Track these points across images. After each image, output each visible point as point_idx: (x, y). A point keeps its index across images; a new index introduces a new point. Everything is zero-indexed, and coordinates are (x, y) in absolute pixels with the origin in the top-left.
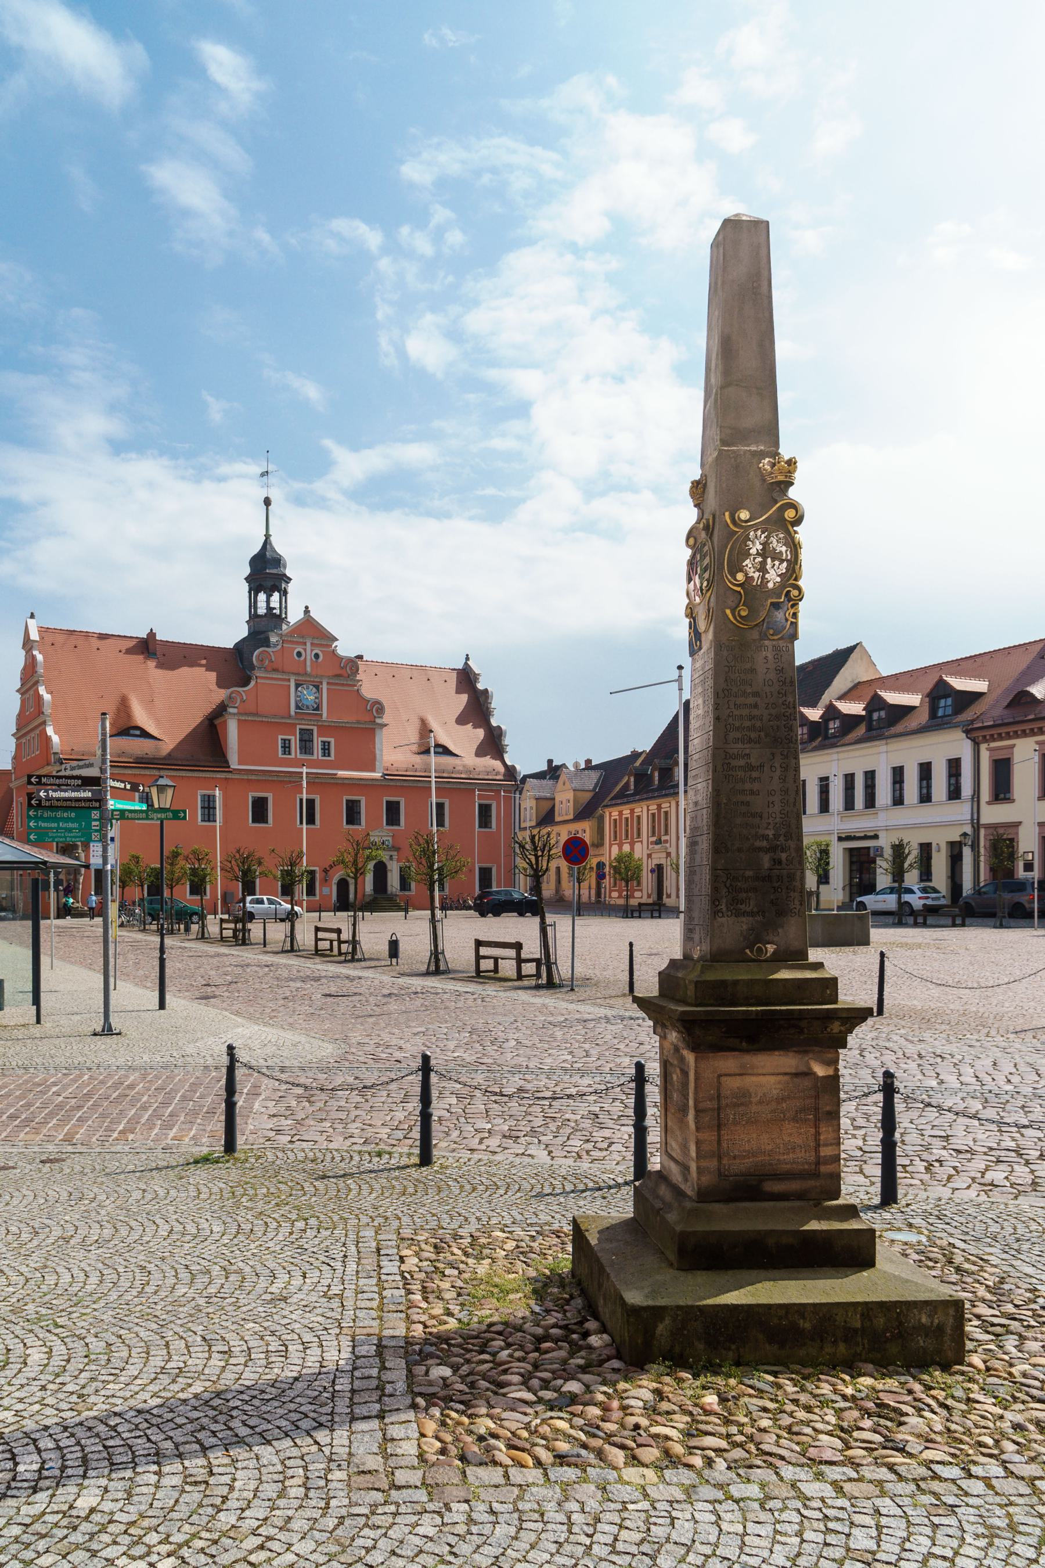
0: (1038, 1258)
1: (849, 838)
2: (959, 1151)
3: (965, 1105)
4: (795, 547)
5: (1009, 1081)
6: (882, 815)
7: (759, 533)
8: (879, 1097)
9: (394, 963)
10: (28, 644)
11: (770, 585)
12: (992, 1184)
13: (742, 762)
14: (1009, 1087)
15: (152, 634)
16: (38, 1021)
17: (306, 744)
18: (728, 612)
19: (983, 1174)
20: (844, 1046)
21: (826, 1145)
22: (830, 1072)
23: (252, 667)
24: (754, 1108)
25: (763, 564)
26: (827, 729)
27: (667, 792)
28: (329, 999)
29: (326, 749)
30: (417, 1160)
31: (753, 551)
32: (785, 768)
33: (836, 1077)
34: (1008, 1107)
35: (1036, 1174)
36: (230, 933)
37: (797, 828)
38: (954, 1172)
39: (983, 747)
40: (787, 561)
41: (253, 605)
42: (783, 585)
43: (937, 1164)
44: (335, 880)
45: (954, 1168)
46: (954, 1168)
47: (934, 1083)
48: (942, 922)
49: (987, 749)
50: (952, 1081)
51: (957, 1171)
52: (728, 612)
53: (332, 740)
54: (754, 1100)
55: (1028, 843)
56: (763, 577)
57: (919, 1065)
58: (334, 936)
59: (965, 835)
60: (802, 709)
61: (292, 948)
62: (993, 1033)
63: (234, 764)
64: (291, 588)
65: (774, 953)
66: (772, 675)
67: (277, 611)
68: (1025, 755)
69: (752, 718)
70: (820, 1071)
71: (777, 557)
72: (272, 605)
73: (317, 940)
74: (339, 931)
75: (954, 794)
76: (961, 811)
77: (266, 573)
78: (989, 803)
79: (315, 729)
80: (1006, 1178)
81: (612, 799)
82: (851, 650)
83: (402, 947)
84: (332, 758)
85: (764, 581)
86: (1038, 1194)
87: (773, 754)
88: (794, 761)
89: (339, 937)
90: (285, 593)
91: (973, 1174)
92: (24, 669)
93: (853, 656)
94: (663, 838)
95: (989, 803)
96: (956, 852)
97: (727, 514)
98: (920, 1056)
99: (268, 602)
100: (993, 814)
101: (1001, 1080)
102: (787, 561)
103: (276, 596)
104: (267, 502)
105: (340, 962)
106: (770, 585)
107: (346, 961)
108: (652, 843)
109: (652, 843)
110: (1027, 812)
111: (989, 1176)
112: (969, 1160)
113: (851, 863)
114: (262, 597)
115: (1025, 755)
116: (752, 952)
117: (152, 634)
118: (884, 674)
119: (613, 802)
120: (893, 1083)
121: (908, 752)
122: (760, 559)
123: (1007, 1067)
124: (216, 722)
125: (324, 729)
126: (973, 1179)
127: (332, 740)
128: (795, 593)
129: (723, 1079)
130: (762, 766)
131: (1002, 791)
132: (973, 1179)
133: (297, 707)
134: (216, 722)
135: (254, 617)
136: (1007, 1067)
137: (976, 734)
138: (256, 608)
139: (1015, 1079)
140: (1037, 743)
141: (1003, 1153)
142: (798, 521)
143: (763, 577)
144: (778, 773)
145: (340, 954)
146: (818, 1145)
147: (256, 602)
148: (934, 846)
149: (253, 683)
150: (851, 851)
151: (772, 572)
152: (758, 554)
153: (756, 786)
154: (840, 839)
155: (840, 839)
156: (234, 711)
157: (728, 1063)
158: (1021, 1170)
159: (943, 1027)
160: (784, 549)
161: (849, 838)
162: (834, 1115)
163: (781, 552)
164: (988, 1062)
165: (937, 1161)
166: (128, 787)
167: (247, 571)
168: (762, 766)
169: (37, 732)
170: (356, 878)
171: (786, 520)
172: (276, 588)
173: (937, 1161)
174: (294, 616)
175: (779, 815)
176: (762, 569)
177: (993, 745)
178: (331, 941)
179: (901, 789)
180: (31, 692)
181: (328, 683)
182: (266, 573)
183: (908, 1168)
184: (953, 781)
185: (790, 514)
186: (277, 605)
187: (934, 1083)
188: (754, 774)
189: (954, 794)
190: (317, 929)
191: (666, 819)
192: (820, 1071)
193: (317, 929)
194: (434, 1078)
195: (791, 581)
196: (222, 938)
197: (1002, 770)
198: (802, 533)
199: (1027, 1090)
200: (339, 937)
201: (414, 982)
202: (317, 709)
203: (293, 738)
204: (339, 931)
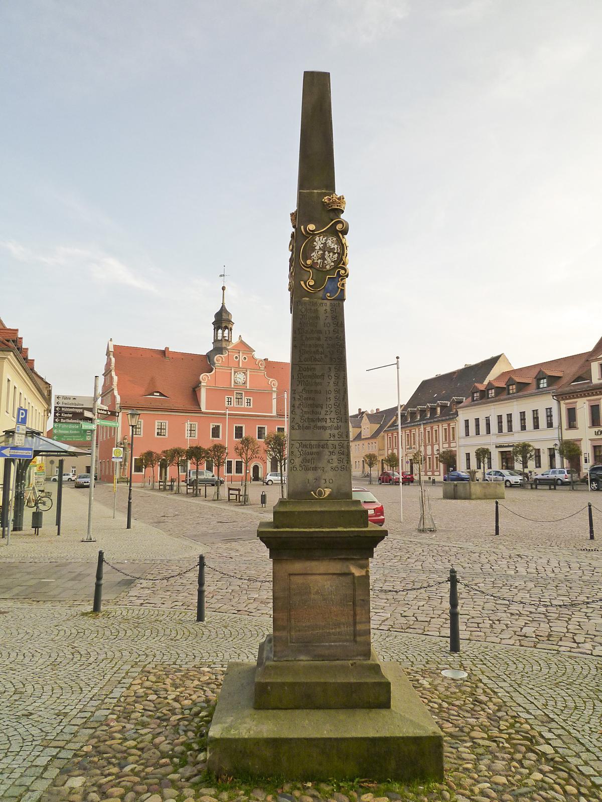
0: (529, 691)
1: (501, 447)
2: (512, 614)
3: (525, 585)
4: (343, 246)
5: (553, 571)
6: (516, 435)
7: (321, 237)
8: (449, 585)
9: (264, 506)
10: (108, 354)
11: (328, 267)
12: (525, 636)
13: (310, 373)
14: (553, 575)
15: (167, 348)
16: (59, 534)
17: (239, 399)
18: (302, 283)
19: (522, 629)
20: (372, 556)
21: (360, 623)
22: (363, 573)
23: (214, 364)
24: (312, 596)
25: (323, 254)
26: (488, 394)
27: (414, 424)
28: (220, 524)
29: (249, 403)
30: (196, 618)
31: (317, 248)
32: (337, 377)
33: (367, 577)
34: (549, 587)
35: (552, 629)
36: (191, 491)
37: (345, 414)
38: (505, 628)
39: (562, 402)
40: (338, 253)
41: (216, 335)
42: (336, 267)
43: (497, 622)
44: (252, 466)
45: (506, 625)
46: (506, 625)
47: (512, 573)
48: (545, 488)
49: (564, 404)
50: (522, 571)
51: (507, 627)
52: (302, 283)
53: (251, 398)
54: (312, 592)
55: (586, 449)
56: (323, 263)
57: (508, 562)
58: (237, 492)
59: (556, 445)
60: (476, 384)
61: (217, 499)
62: (553, 544)
63: (203, 409)
64: (234, 327)
65: (329, 495)
66: (329, 320)
67: (227, 338)
68: (583, 407)
69: (316, 346)
70: (357, 572)
71: (331, 250)
72: (225, 335)
73: (229, 494)
74: (239, 490)
75: (550, 425)
76: (554, 433)
77: (222, 321)
78: (566, 429)
79: (243, 393)
80: (534, 632)
81: (388, 427)
82: (497, 358)
83: (267, 499)
84: (251, 407)
85: (324, 266)
86: (550, 642)
87: (330, 368)
88: (343, 373)
89: (239, 493)
90: (231, 329)
91: (515, 629)
92: (106, 364)
93: (500, 359)
94: (413, 446)
95: (566, 429)
96: (552, 453)
97: (302, 227)
98: (510, 557)
99: (223, 334)
100: (569, 435)
101: (549, 569)
102: (338, 253)
103: (227, 331)
104: (223, 288)
105: (236, 505)
106: (328, 267)
107: (241, 505)
108: (408, 449)
109: (408, 449)
110: (585, 435)
111: (525, 630)
112: (517, 620)
113: (502, 459)
114: (220, 331)
115: (583, 407)
116: (315, 494)
117: (167, 348)
118: (515, 368)
119: (389, 429)
120: (455, 576)
121: (528, 405)
122: (321, 252)
123: (554, 563)
124: (196, 389)
125: (248, 393)
126: (515, 632)
127: (251, 398)
128: (342, 272)
129: (292, 578)
130: (323, 375)
131: (572, 424)
132: (515, 632)
133: (235, 382)
134: (196, 389)
135: (216, 341)
136: (554, 563)
137: (560, 397)
138: (217, 337)
139: (557, 570)
140: (588, 401)
141: (537, 615)
142: (345, 232)
143: (323, 263)
144: (333, 380)
145: (239, 502)
146: (355, 624)
147: (217, 334)
148: (541, 450)
149: (214, 371)
150: (502, 452)
151: (329, 259)
152: (320, 249)
153: (319, 388)
154: (496, 447)
155: (496, 447)
156: (205, 384)
157: (298, 566)
158: (544, 626)
159: (529, 541)
160: (336, 246)
161: (501, 447)
162: (366, 602)
163: (334, 248)
164: (544, 561)
165: (498, 620)
166: (109, 413)
167: (213, 320)
168: (323, 375)
169: (110, 394)
170: (246, 463)
171: (339, 232)
172: (226, 328)
173: (498, 620)
174: (235, 340)
175: (333, 406)
176: (323, 257)
177: (567, 401)
178: (237, 495)
179: (525, 423)
180: (109, 375)
181: (250, 372)
182: (222, 321)
183: (480, 625)
184: (549, 419)
185: (339, 227)
186: (227, 335)
187: (512, 573)
188: (318, 381)
189: (550, 425)
190: (230, 489)
191: (414, 437)
192: (357, 572)
193: (230, 489)
194: (206, 569)
195: (340, 265)
196: (187, 493)
197: (572, 413)
198: (348, 239)
199: (561, 577)
200: (239, 493)
201: (267, 516)
202: (244, 383)
203: (232, 397)
204: (239, 490)
